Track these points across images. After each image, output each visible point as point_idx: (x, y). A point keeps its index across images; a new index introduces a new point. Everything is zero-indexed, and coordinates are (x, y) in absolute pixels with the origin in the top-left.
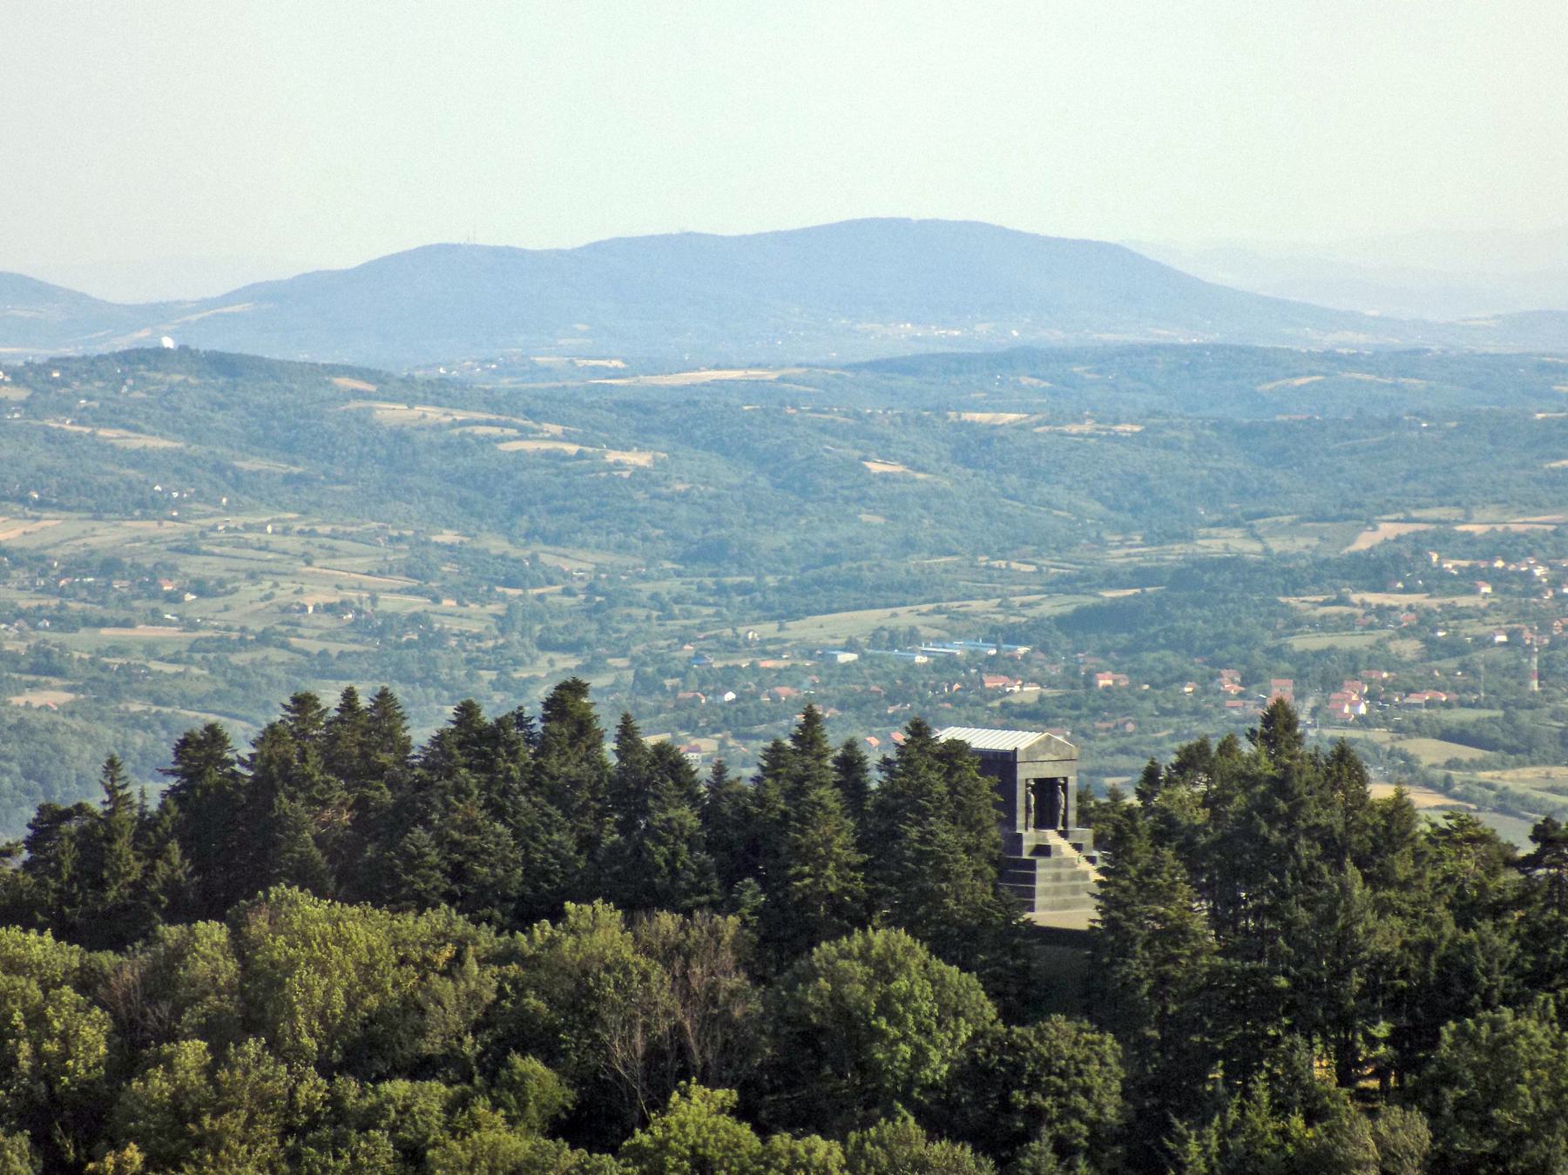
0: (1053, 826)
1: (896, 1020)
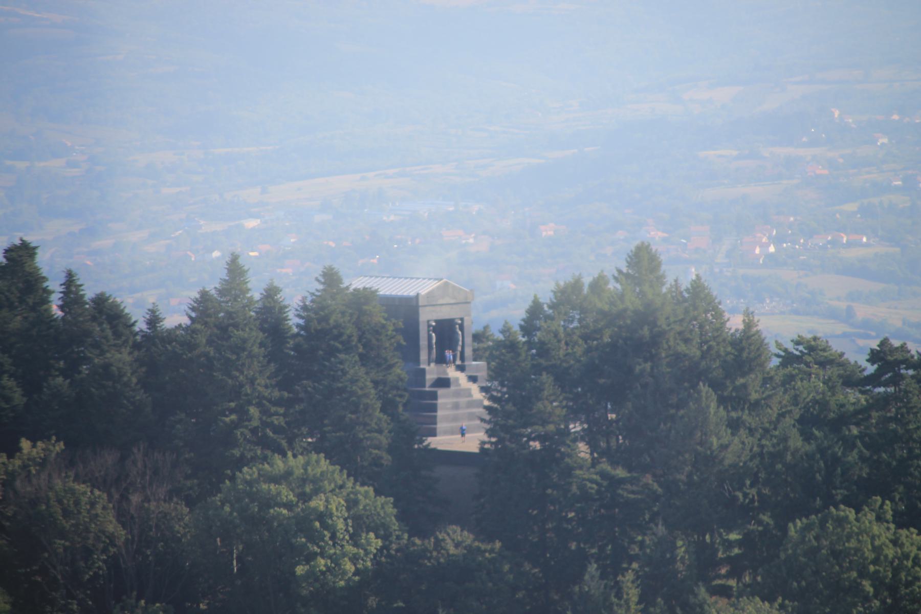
1: (314, 537)
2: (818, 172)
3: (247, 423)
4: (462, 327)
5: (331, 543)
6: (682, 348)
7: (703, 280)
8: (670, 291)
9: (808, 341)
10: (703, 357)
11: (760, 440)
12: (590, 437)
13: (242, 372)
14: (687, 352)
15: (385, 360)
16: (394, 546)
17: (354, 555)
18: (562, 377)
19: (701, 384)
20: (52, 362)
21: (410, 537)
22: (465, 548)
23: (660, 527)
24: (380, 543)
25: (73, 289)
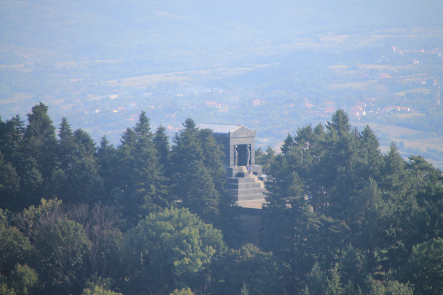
0: (245, 164)
1: (183, 248)
2: (386, 77)
3: (149, 193)
4: (250, 149)
5: (191, 250)
6: (360, 160)
7: (370, 128)
8: (352, 133)
9: (416, 158)
10: (370, 165)
11: (398, 205)
12: (312, 202)
13: (147, 168)
14: (363, 162)
15: (216, 163)
16: (221, 253)
17: (202, 256)
18: (302, 173)
19: (370, 178)
20: (55, 161)
21: (229, 249)
22: (256, 254)
23: (350, 246)
24: (215, 251)
25: (66, 127)
